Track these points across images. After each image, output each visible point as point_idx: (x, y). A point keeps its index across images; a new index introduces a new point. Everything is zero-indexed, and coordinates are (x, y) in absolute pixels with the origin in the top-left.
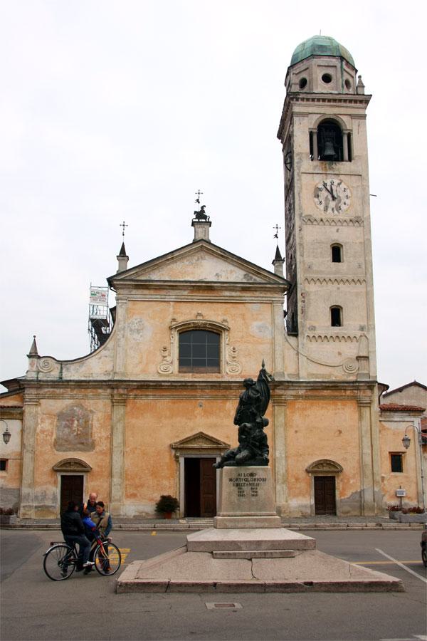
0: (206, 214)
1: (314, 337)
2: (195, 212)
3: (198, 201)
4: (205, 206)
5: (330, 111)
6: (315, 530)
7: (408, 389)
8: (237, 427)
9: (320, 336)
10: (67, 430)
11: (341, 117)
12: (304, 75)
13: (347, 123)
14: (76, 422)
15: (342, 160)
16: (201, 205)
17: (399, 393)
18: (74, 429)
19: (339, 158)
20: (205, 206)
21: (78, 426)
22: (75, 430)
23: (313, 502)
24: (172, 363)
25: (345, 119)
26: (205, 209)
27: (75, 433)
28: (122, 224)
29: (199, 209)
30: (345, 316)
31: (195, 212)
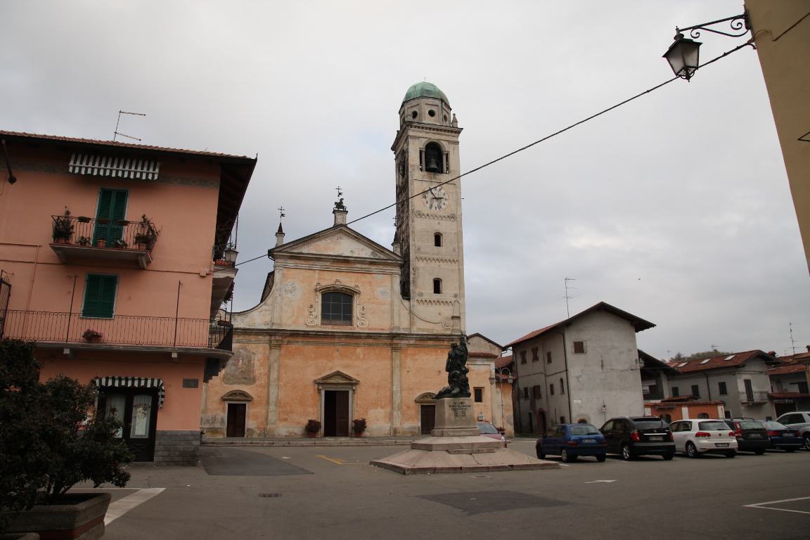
2: (336, 203)
5: (434, 137)
9: (446, 302)
11: (442, 142)
14: (241, 361)
26: (343, 201)
30: (443, 286)
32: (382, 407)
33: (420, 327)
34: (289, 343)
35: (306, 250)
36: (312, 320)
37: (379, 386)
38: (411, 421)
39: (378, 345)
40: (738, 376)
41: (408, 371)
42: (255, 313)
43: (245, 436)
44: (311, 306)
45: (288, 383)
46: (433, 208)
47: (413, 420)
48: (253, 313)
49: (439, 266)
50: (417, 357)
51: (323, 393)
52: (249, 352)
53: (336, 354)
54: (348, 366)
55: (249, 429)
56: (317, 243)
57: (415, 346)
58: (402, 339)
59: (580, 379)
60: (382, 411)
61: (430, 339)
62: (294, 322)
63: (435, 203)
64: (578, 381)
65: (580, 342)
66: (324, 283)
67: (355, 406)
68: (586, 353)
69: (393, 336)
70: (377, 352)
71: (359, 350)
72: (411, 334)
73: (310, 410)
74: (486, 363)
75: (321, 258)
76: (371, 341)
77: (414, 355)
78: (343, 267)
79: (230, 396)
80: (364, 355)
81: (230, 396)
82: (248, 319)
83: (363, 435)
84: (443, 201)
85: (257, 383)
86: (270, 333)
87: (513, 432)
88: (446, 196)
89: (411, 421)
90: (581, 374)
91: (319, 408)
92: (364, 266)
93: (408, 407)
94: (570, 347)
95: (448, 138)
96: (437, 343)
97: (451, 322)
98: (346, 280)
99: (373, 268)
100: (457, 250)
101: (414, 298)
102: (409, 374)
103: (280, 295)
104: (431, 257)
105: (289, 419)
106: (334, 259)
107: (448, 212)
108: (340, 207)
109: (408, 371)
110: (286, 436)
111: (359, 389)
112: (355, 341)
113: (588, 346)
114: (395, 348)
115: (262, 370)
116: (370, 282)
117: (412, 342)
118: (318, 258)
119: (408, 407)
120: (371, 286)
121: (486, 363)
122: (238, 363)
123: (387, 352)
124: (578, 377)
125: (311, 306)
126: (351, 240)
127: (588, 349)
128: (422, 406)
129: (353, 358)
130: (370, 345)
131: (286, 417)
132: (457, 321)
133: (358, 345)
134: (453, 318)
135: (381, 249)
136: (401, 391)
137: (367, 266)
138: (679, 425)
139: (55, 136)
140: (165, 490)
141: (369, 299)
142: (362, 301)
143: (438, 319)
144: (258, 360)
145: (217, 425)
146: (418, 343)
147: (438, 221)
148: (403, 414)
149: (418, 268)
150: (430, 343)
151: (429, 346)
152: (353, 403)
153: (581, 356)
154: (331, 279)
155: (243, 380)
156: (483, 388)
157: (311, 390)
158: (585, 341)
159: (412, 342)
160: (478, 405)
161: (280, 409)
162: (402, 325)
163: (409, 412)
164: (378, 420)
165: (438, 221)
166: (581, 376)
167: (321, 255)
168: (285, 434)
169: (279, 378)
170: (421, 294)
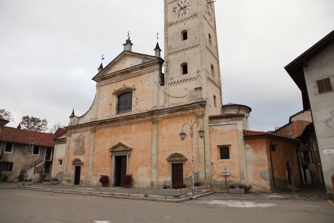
14: (80, 142)
32: (146, 166)
33: (174, 102)
34: (99, 128)
36: (111, 113)
37: (144, 151)
38: (164, 177)
39: (144, 121)
41: (163, 138)
42: (87, 115)
43: (80, 184)
44: (111, 104)
45: (98, 153)
46: (181, 16)
47: (166, 176)
48: (86, 115)
49: (185, 53)
50: (169, 126)
51: (113, 157)
52: (84, 137)
53: (121, 132)
54: (126, 139)
55: (81, 181)
56: (115, 67)
57: (168, 118)
58: (158, 114)
59: (330, 123)
60: (146, 169)
61: (178, 110)
62: (103, 116)
63: (182, 12)
64: (328, 126)
65: (325, 80)
66: (117, 89)
67: (129, 164)
69: (152, 113)
70: (143, 126)
71: (133, 127)
72: (164, 109)
73: (107, 169)
74: (230, 123)
75: (115, 75)
76: (140, 119)
77: (167, 125)
78: (127, 75)
79: (75, 162)
80: (136, 130)
81: (75, 162)
82: (84, 119)
83: (249, 191)
84: (187, 8)
85: (86, 154)
86: (90, 124)
87: (269, 187)
88: (190, 3)
89: (164, 177)
90: (331, 116)
91: (111, 168)
92: (137, 71)
93: (163, 166)
96: (184, 113)
97: (195, 93)
98: (129, 83)
99: (143, 71)
100: (198, 37)
101: (166, 82)
102: (164, 139)
103: (97, 102)
104: (179, 50)
105: (98, 175)
106: (121, 73)
107: (192, 13)
108: (129, 42)
109: (163, 138)
110: (96, 185)
111: (133, 154)
112: (131, 121)
114: (154, 122)
115: (88, 146)
116: (142, 80)
117: (166, 115)
118: (114, 75)
119: (163, 166)
120: (142, 83)
121: (230, 123)
122: (79, 143)
123: (149, 125)
124: (326, 122)
125: (111, 104)
126: (131, 58)
128: (172, 164)
129: (130, 132)
130: (139, 122)
131: (96, 173)
132: (199, 91)
133: (132, 124)
134: (196, 89)
135: (144, 56)
136: (158, 153)
137: (139, 71)
138: (323, 185)
141: (141, 92)
142: (136, 94)
143: (185, 93)
144: (87, 141)
145: (71, 178)
146: (170, 115)
147: (184, 23)
148: (159, 171)
149: (170, 61)
150: (179, 113)
151: (177, 116)
152: (128, 164)
154: (119, 86)
155: (81, 153)
156: (230, 145)
157: (108, 154)
159: (166, 115)
160: (223, 162)
161: (94, 169)
162: (161, 104)
163: (163, 170)
164: (143, 176)
165: (184, 23)
168: (96, 184)
169: (94, 150)
170: (172, 78)
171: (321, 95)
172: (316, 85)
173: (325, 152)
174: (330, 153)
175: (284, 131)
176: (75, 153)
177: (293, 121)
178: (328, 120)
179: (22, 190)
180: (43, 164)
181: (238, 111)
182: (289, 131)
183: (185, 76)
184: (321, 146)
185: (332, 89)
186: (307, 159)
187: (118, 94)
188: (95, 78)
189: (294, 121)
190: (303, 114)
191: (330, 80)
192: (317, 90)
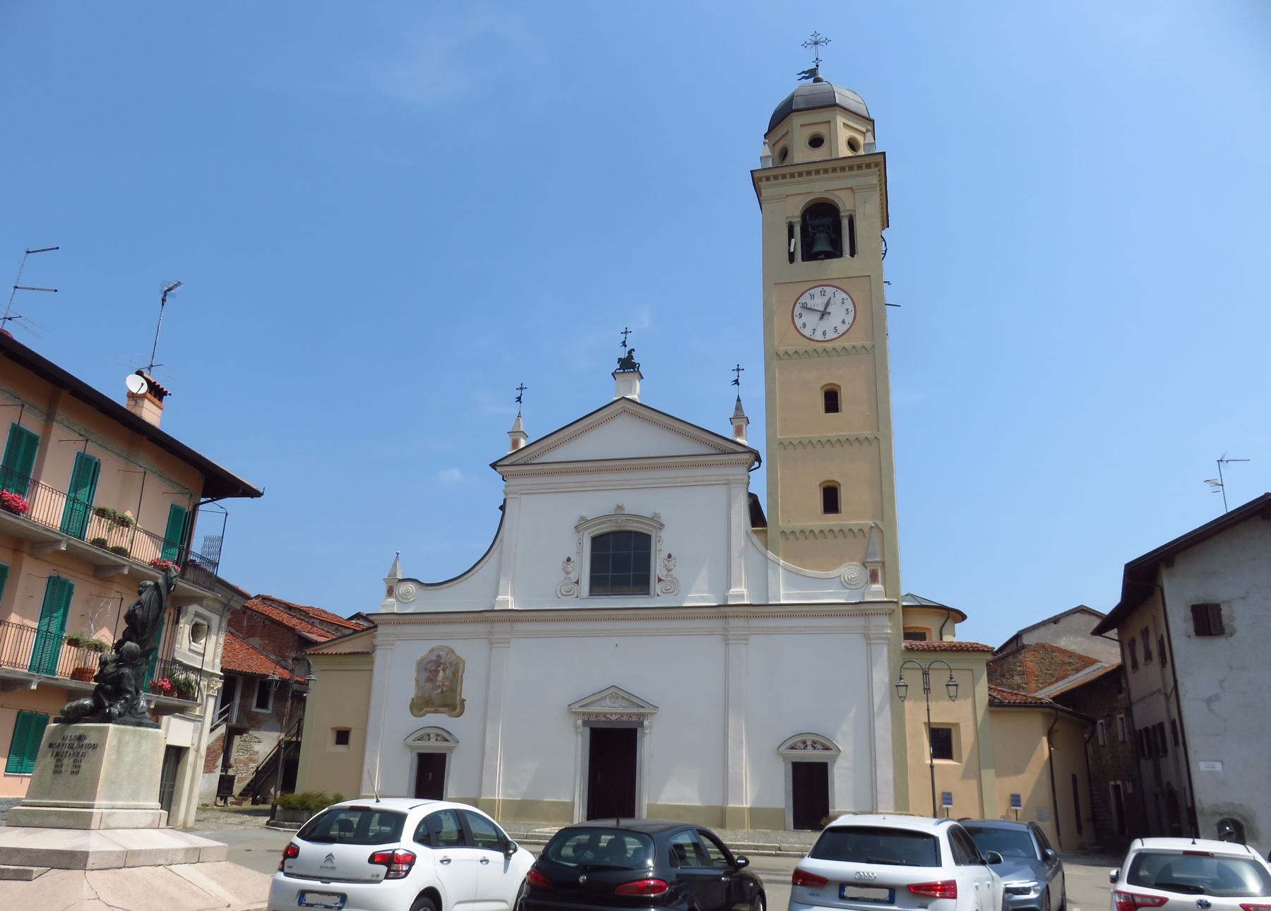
0: (636, 360)
1: (841, 530)
2: (620, 360)
3: (624, 344)
4: (634, 350)
5: (819, 188)
6: (776, 855)
7: (1068, 618)
8: (1150, 727)
9: (812, 531)
10: (429, 685)
11: (836, 193)
12: (821, 129)
13: (845, 203)
14: (441, 674)
15: (840, 255)
16: (628, 349)
17: (1054, 626)
18: (438, 684)
19: (836, 253)
20: (634, 350)
21: (443, 678)
22: (439, 686)
23: (830, 810)
24: (577, 582)
25: (841, 194)
26: (634, 354)
27: (440, 690)
28: (524, 386)
29: (624, 355)
30: (844, 497)
31: (620, 360)
35: (500, 464)
40: (704, 845)
64: (1210, 710)
68: (1235, 631)
94: (1179, 621)
95: (849, 183)
113: (1238, 615)
122: (436, 676)
124: (1209, 701)
127: (1235, 624)
139: (8, 333)
140: (576, 866)
153: (1217, 645)
158: (1228, 602)
166: (1218, 697)
167: (93, 498)
171: (843, 408)
172: (1190, 615)
173: (1203, 766)
174: (1214, 770)
175: (999, 671)
176: (420, 706)
177: (1025, 643)
178: (1213, 698)
179: (286, 833)
180: (219, 738)
181: (943, 622)
182: (1014, 672)
183: (832, 520)
184: (1195, 752)
185: (1224, 630)
186: (304, 612)
187: (593, 532)
188: (500, 464)
189: (1029, 643)
190: (1055, 625)
191: (1221, 609)
192: (1191, 627)
